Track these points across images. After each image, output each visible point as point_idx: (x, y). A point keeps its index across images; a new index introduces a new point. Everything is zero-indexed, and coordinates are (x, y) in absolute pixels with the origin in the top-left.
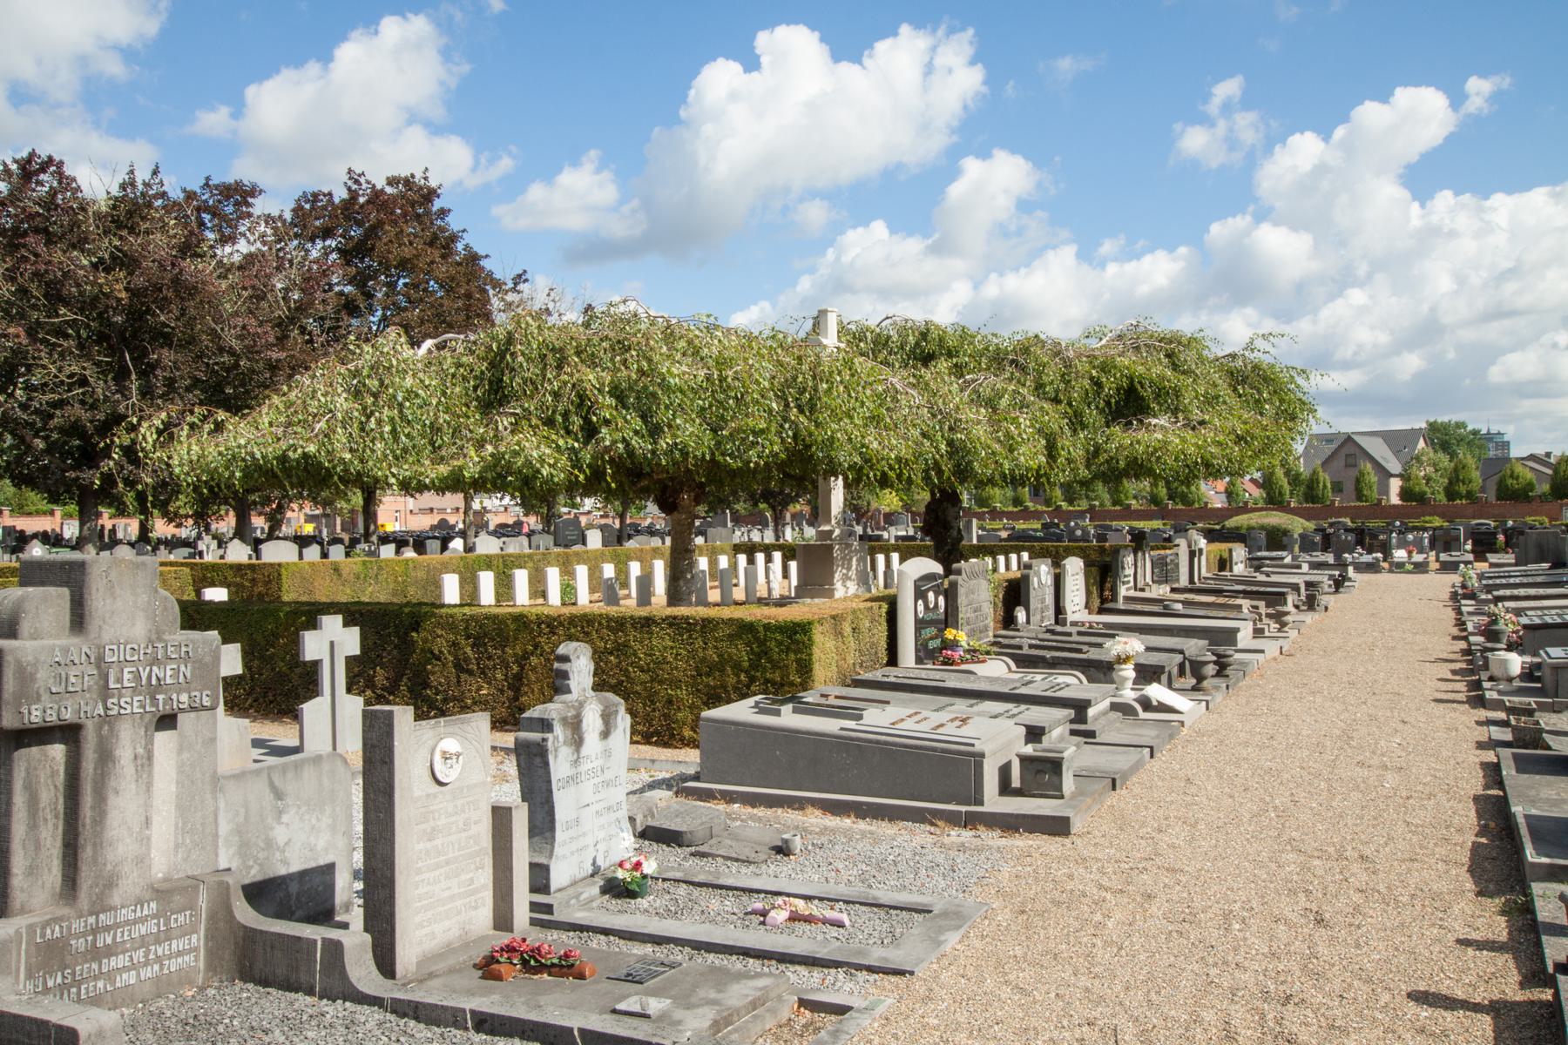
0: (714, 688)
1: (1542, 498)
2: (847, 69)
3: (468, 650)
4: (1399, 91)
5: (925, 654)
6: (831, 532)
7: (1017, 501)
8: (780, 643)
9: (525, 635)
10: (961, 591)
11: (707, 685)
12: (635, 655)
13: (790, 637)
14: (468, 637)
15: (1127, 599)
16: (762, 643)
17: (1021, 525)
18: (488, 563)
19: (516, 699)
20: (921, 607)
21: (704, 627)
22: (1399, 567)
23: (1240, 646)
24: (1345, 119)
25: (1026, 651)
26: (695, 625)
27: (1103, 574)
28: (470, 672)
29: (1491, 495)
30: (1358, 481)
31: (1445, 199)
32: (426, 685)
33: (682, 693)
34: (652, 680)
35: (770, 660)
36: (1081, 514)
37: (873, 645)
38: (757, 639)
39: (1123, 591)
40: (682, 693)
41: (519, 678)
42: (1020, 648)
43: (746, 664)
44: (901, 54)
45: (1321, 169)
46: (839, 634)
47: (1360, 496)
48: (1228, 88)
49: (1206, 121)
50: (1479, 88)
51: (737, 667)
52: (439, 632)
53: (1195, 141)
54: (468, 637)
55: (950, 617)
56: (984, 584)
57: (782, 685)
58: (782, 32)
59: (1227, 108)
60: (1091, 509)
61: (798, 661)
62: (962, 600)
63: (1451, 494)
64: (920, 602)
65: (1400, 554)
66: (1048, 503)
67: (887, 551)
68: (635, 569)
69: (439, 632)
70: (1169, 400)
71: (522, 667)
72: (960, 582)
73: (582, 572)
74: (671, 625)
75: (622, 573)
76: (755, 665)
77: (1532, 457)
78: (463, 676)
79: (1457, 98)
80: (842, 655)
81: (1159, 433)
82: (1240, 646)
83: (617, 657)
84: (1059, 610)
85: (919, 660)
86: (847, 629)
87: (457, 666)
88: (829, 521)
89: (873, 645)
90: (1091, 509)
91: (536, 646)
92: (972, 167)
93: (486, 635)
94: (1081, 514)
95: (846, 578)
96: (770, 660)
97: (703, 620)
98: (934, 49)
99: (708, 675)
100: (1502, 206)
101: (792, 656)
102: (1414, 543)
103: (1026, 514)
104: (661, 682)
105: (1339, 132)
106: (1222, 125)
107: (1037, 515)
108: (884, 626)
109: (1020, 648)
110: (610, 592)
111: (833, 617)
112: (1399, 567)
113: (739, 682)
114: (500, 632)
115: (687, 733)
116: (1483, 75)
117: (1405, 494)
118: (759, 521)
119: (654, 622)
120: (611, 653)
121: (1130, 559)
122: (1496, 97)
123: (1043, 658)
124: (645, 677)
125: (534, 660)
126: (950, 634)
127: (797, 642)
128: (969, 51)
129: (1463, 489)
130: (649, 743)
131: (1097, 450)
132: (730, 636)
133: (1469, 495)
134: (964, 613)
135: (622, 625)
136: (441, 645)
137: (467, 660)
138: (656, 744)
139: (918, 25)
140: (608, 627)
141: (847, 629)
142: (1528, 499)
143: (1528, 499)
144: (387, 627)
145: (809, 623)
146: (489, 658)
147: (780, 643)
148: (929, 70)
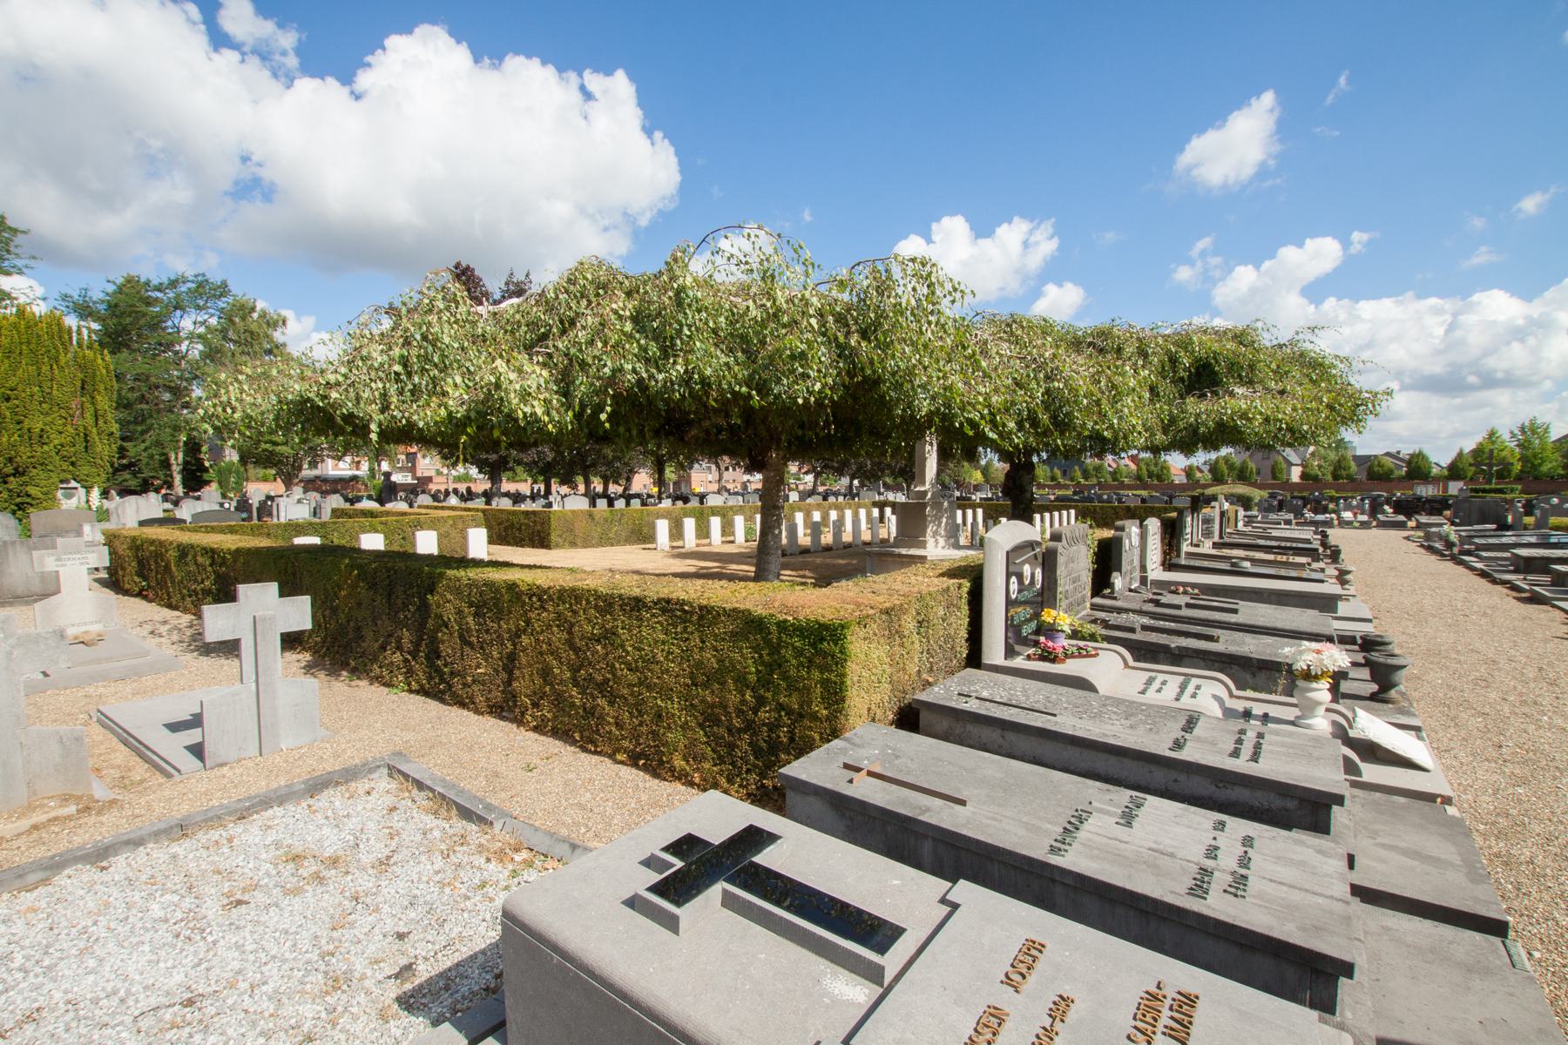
0: (713, 706)
1: (1401, 479)
2: (985, 243)
3: (470, 619)
4: (1308, 241)
5: (1015, 639)
6: (925, 493)
7: (1053, 478)
8: (799, 653)
9: (516, 608)
10: (1061, 560)
11: (703, 701)
12: (623, 646)
13: (813, 645)
14: (471, 605)
15: (1189, 554)
16: (775, 649)
17: (1059, 493)
18: (715, 511)
19: (509, 683)
20: (1014, 586)
21: (701, 617)
22: (1349, 524)
23: (1340, 613)
24: (1272, 256)
25: (1139, 636)
26: (691, 613)
27: (1172, 532)
28: (470, 645)
29: (1363, 477)
30: (1273, 468)
31: (1330, 303)
32: (439, 657)
33: (674, 707)
34: (641, 684)
35: (785, 677)
36: (1093, 486)
37: (948, 638)
38: (768, 642)
39: (1186, 547)
40: (674, 707)
41: (512, 657)
42: (1132, 630)
43: (752, 678)
44: (1012, 234)
45: (1253, 291)
46: (894, 634)
47: (1274, 477)
48: (1204, 243)
49: (1191, 263)
50: (1358, 237)
51: (741, 680)
52: (449, 596)
53: (1184, 274)
54: (471, 605)
55: (1047, 595)
56: (1083, 549)
57: (801, 716)
58: (946, 221)
59: (1203, 254)
60: (1099, 484)
61: (825, 683)
62: (1061, 571)
63: (1336, 477)
64: (1014, 579)
65: (1347, 515)
66: (1072, 479)
67: (974, 507)
68: (833, 515)
69: (449, 596)
70: (1246, 374)
71: (514, 645)
72: (1060, 550)
73: (862, 512)
74: (664, 611)
75: (825, 517)
76: (765, 682)
77: (1388, 454)
78: (467, 649)
79: (1346, 243)
80: (897, 664)
81: (1239, 400)
82: (1340, 613)
83: (604, 647)
84: (1143, 568)
85: (1010, 652)
86: (909, 623)
87: (461, 637)
88: (924, 483)
89: (948, 638)
90: (1099, 484)
91: (528, 622)
92: (1051, 290)
93: (485, 604)
94: (1093, 486)
95: (935, 534)
96: (785, 677)
97: (701, 608)
98: (1031, 232)
99: (705, 686)
100: (1367, 308)
101: (816, 675)
102: (1357, 507)
103: (1060, 486)
104: (649, 688)
105: (1267, 265)
106: (1199, 264)
107: (1066, 487)
108: (965, 609)
109: (1132, 630)
110: (815, 529)
111: (887, 612)
112: (1349, 524)
113: (743, 702)
114: (497, 602)
115: (679, 762)
116: (1361, 231)
117: (1304, 476)
118: (896, 488)
119: (645, 605)
120: (598, 641)
121: (1189, 519)
122: (1370, 243)
123: (1166, 649)
124: (633, 678)
125: (525, 640)
126: (1048, 616)
127: (825, 654)
128: (1051, 231)
129: (1344, 473)
130: (636, 765)
131: (1173, 420)
132: (734, 634)
133: (1349, 477)
134: (1063, 585)
135: (611, 605)
136: (449, 612)
137: (469, 630)
138: (645, 769)
139: (1024, 216)
140: (596, 607)
141: (909, 623)
142: (1391, 480)
143: (1391, 480)
144: (411, 587)
145: (843, 627)
146: (487, 631)
147: (799, 653)
148: (1026, 244)
